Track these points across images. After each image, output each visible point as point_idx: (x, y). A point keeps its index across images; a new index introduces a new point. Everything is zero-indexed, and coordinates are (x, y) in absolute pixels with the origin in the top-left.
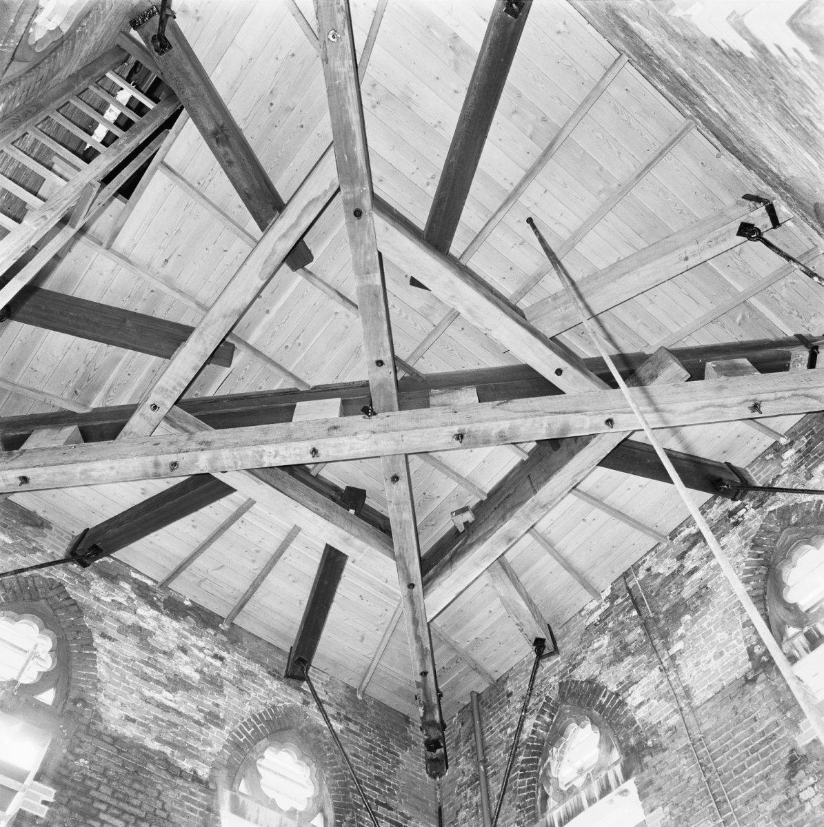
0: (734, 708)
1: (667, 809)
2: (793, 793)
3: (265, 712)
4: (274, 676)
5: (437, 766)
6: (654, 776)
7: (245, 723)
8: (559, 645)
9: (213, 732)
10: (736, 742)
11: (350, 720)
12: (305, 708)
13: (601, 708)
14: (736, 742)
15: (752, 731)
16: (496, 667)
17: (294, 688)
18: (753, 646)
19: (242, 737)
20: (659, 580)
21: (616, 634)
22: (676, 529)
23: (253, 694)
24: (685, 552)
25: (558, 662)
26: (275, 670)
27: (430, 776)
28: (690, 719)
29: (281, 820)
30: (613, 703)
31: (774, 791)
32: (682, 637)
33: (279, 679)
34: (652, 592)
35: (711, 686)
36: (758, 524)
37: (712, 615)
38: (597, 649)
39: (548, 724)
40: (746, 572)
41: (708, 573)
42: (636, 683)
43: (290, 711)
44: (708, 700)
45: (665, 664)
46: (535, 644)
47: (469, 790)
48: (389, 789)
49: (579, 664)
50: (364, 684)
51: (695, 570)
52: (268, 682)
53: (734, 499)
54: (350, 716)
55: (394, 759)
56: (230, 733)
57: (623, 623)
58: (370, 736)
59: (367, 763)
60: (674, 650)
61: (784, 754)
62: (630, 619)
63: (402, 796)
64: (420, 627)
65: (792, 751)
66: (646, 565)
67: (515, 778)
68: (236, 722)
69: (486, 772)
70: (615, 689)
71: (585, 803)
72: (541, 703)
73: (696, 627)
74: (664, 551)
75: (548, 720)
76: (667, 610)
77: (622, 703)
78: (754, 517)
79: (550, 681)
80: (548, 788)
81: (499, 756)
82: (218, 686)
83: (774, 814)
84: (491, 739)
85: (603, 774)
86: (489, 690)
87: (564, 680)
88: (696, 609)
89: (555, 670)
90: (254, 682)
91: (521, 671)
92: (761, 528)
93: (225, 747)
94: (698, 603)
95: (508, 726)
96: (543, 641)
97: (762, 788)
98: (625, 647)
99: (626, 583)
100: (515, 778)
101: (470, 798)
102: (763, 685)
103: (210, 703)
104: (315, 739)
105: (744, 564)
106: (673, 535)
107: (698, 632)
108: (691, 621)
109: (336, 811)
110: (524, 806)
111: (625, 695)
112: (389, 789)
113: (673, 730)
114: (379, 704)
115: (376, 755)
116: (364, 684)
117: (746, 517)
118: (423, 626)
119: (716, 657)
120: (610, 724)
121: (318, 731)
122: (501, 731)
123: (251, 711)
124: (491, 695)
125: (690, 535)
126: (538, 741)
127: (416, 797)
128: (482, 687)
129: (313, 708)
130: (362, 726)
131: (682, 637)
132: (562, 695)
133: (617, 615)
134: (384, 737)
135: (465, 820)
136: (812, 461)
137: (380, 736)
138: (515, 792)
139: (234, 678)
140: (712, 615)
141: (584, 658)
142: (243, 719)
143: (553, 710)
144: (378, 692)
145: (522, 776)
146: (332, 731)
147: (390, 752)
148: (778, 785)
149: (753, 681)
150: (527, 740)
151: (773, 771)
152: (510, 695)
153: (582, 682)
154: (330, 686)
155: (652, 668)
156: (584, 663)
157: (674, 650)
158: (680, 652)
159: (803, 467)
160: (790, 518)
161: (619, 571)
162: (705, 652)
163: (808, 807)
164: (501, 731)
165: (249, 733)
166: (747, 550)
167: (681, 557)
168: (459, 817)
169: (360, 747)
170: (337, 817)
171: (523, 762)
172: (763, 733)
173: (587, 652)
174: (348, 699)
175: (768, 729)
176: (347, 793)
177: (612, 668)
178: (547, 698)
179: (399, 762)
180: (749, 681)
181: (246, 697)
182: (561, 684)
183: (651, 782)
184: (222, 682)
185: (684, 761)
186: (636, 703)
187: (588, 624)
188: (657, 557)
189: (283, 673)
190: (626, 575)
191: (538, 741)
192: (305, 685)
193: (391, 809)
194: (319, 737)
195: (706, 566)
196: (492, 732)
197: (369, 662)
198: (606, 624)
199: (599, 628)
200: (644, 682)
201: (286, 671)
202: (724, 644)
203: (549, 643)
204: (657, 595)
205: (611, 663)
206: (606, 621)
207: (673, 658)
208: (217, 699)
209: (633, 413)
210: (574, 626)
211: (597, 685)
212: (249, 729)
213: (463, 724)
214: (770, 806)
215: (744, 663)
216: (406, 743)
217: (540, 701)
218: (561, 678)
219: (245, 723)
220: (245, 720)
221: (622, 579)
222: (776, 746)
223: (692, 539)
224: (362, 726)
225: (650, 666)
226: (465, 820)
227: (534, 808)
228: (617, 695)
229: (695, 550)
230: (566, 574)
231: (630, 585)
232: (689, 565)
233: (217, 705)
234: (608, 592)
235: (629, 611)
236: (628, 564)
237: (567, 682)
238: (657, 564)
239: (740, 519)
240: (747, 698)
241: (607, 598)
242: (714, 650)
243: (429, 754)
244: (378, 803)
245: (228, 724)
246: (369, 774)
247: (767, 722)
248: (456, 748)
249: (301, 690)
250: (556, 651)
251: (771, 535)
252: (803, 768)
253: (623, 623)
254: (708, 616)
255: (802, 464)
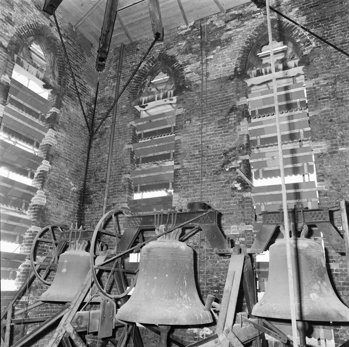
0: (222, 86)
1: (185, 109)
2: (228, 117)
3: (33, 24)
4: (38, 8)
5: (100, 67)
6: (184, 98)
7: (23, 27)
8: (164, 38)
9: (9, 27)
10: (217, 97)
11: (69, 39)
12: (50, 28)
13: (173, 68)
14: (217, 97)
15: (224, 95)
16: (135, 37)
17: (47, 17)
18: (238, 67)
19: (22, 33)
20: (214, 28)
21: (189, 42)
22: (230, 9)
23: (28, 14)
24: (229, 21)
25: (162, 44)
26: (38, 6)
27: (97, 70)
28: (205, 84)
29: (37, 72)
30: (179, 68)
31: (222, 115)
32: (214, 54)
33: (40, 10)
34: (210, 31)
35: (216, 75)
36: (262, 22)
37: (228, 50)
38: (180, 45)
39: (151, 67)
40: (248, 39)
41: (234, 33)
42: (190, 64)
43: (44, 27)
44: (214, 80)
45: (204, 61)
46: (155, 35)
47: (112, 80)
48: (80, 71)
49: (170, 48)
50: (78, 25)
51: (230, 30)
52: (35, 10)
53: (258, 7)
54: (69, 37)
55: (84, 60)
56: (17, 29)
57: (193, 39)
58: (76, 48)
59: (73, 58)
60: (209, 58)
61: (231, 106)
62: (197, 39)
63: (85, 75)
64: (113, 12)
65: (233, 105)
66: (212, 19)
67: (132, 82)
68: (19, 25)
69: (120, 76)
70: (181, 64)
71: (156, 98)
72: (150, 58)
73: (221, 52)
74: (221, 16)
75: (151, 65)
76: (213, 41)
77: (182, 70)
78: (262, 18)
79: (156, 51)
80: (144, 89)
81: (127, 72)
82: (11, 5)
83: (219, 121)
84: (125, 64)
85: (166, 91)
86: (129, 45)
87: (162, 53)
88: (223, 46)
89: (160, 47)
90: (28, 9)
91: (145, 42)
92: (262, 24)
93: (14, 35)
94: (225, 43)
95: (134, 62)
96: (160, 34)
97: (219, 113)
98: (191, 49)
99: (201, 24)
100: (132, 82)
101: (112, 83)
102: (235, 82)
103: (7, 12)
104: (54, 43)
105: (249, 36)
106: (228, 11)
107: (220, 55)
108: (220, 49)
109: (59, 74)
110: (132, 92)
111: (184, 67)
112: (80, 71)
113: (197, 85)
114: (82, 35)
115: (78, 57)
116: (78, 25)
117: (259, 17)
118: (114, 12)
119: (223, 66)
120: (175, 75)
121: (56, 39)
122: (130, 63)
123: (26, 22)
124: (130, 47)
125: (234, 14)
126: (145, 72)
127: (90, 76)
128: (127, 43)
129: (54, 29)
130: (73, 43)
131: (214, 54)
132: (159, 58)
133: (192, 35)
134: (82, 50)
135: (107, 90)
136: (295, 5)
137: (80, 49)
138: (130, 86)
139: (19, 3)
140: (228, 50)
141: (173, 47)
142: (23, 25)
143: (154, 62)
144: (83, 30)
145: (134, 82)
146: (62, 41)
147: (83, 56)
148: (224, 114)
149: (232, 79)
150: (140, 70)
151: (224, 109)
152: (138, 50)
153: (169, 56)
154: (62, 21)
155: (198, 61)
156: (172, 49)
157: (209, 58)
158: (211, 59)
159: (290, 6)
160: (274, 25)
161: (200, 17)
162: (220, 63)
163: (230, 123)
164: (130, 63)
165: (26, 32)
166: (253, 31)
167: (227, 22)
168: (105, 88)
169: (72, 51)
170: (59, 76)
171: (136, 77)
172: (227, 97)
173: (175, 45)
174: (69, 29)
175: (229, 96)
176: (64, 68)
177: (183, 55)
178: (153, 57)
179: (86, 61)
180: (231, 78)
181: (24, 14)
182: (160, 54)
183: (182, 100)
184: (13, 3)
185: (197, 97)
186: (187, 71)
187: (179, 34)
188: (217, 18)
189: (42, 8)
190: (202, 20)
191: (145, 72)
192: (52, 17)
193: (80, 79)
194: (56, 42)
195: (235, 30)
196: (127, 62)
197: (83, 16)
198: (186, 37)
199: (183, 37)
200: (193, 65)
201: (44, 8)
202: (227, 63)
203: (161, 36)
204: (211, 34)
205: (183, 53)
206: (187, 36)
207: (207, 60)
208: (11, 11)
209: (270, 8)
210: (173, 33)
211: (175, 59)
212: (26, 30)
213: (115, 54)
214: (218, 119)
215: (231, 72)
216: (90, 55)
217: (150, 57)
218: (161, 51)
219: (23, 27)
220: (24, 25)
221: (200, 21)
222: (229, 102)
223: (234, 16)
224: (73, 43)
225: (197, 60)
226: (107, 90)
227: (136, 94)
228: (181, 66)
229: (233, 22)
230: (179, 10)
231: (202, 25)
232: (228, 27)
233: (11, 14)
234: (192, 24)
235: (197, 36)
236: (205, 15)
237: (163, 54)
238: (216, 20)
239: (256, 17)
240: (227, 84)
241: (191, 26)
242: (223, 63)
243: (99, 62)
244: (76, 75)
245: (16, 25)
246: (74, 63)
247: (230, 94)
248: (110, 63)
249: (49, 19)
250: (162, 40)
251: (264, 28)
252: (234, 112)
253: (193, 39)
254: (227, 50)
255: (290, 4)
